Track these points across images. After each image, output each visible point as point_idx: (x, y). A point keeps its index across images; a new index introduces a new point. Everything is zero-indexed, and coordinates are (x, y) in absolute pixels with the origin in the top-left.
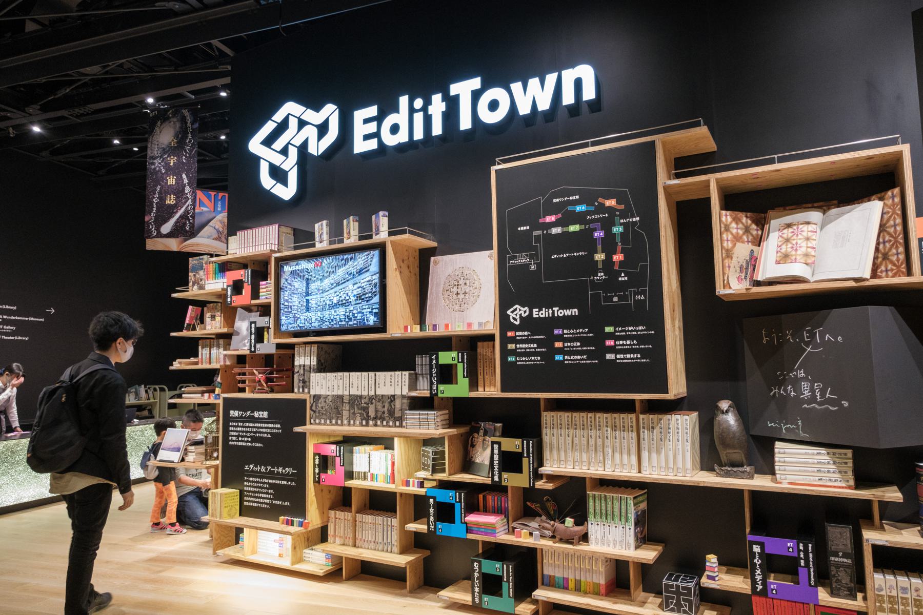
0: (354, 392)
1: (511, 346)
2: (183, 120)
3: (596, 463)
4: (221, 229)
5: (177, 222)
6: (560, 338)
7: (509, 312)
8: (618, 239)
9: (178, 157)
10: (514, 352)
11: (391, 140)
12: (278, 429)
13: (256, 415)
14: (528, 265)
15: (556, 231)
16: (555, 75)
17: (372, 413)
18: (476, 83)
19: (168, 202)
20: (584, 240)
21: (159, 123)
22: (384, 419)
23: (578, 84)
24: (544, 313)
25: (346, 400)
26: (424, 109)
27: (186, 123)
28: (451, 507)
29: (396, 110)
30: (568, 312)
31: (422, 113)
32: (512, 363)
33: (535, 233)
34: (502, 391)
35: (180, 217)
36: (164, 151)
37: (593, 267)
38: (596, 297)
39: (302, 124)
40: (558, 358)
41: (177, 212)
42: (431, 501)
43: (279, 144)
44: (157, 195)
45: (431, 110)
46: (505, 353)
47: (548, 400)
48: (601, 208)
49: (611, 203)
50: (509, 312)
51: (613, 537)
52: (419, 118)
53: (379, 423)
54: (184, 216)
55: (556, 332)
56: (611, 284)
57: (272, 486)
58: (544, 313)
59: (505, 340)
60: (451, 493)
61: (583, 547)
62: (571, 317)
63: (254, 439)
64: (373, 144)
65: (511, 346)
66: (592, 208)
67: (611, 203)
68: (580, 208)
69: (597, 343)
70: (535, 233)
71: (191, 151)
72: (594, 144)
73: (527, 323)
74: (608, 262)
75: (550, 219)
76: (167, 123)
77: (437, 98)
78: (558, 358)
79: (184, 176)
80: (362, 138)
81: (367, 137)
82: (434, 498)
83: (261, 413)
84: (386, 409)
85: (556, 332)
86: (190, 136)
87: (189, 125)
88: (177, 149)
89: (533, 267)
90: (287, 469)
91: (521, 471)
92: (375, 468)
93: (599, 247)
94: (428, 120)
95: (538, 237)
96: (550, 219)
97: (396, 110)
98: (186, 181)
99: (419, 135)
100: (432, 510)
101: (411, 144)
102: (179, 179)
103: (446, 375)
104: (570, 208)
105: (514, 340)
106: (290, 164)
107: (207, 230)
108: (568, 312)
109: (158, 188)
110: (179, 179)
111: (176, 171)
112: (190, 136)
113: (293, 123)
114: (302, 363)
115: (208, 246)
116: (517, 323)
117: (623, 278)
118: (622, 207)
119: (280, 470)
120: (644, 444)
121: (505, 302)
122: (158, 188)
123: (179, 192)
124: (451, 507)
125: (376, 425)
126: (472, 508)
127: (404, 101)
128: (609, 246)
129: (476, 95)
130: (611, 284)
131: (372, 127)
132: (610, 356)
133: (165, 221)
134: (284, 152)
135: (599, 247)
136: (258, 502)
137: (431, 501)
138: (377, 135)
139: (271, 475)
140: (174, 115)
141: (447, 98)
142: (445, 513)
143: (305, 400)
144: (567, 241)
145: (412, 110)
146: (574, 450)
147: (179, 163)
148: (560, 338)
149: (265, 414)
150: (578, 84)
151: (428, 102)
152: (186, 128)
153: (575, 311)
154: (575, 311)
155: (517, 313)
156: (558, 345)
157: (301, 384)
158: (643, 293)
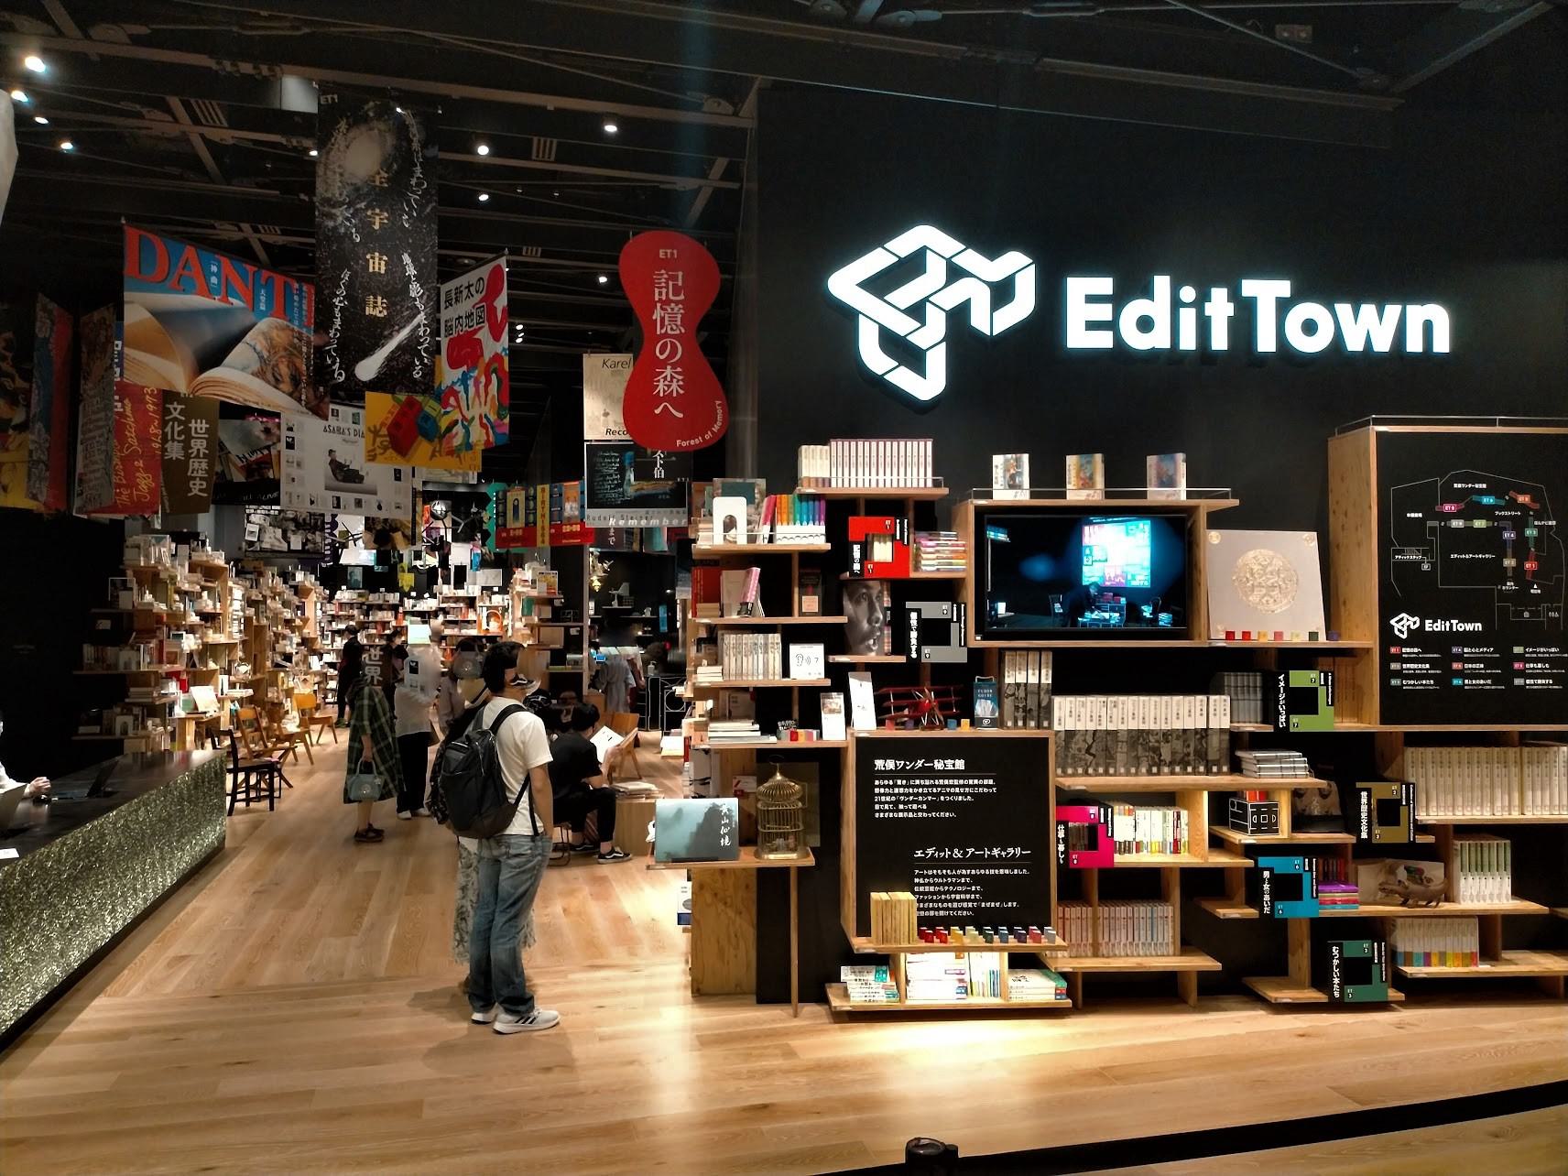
0: (1133, 726)
1: (1394, 666)
2: (401, 129)
3: (1543, 806)
4: (266, 354)
5: (390, 359)
6: (1460, 658)
7: (1393, 622)
8: (1531, 544)
9: (392, 212)
10: (1399, 674)
11: (1138, 341)
12: (988, 786)
13: (938, 765)
14: (1419, 563)
15: (1457, 524)
16: (1399, 308)
17: (1166, 755)
18: (1283, 288)
19: (369, 311)
20: (1490, 540)
21: (343, 125)
22: (1188, 764)
23: (1428, 327)
24: (1439, 626)
25: (1123, 737)
26: (1199, 304)
27: (410, 141)
28: (1297, 879)
29: (1147, 293)
30: (1469, 627)
31: (1193, 311)
32: (1396, 687)
33: (1429, 523)
34: (1383, 722)
35: (399, 347)
36: (357, 193)
37: (1502, 575)
38: (1504, 611)
39: (955, 273)
40: (1456, 682)
41: (391, 336)
42: (1266, 874)
43: (907, 294)
44: (342, 291)
45: (1209, 309)
46: (1386, 674)
47: (1407, 734)
48: (1513, 504)
49: (1523, 499)
50: (1393, 622)
51: (1487, 891)
52: (1188, 317)
53: (1177, 769)
54: (409, 347)
55: (1455, 650)
56: (1522, 597)
57: (976, 880)
58: (1439, 626)
59: (1386, 658)
60: (1298, 861)
61: (1446, 907)
62: (1474, 632)
63: (933, 806)
64: (1104, 340)
65: (1394, 666)
66: (1502, 503)
67: (1523, 499)
68: (1488, 500)
69: (1503, 666)
70: (1429, 523)
71: (422, 206)
72: (1503, 423)
73: (1417, 637)
74: (1519, 569)
75: (1448, 508)
76: (363, 128)
77: (1219, 294)
78: (1456, 682)
79: (406, 259)
80: (1083, 326)
81: (1092, 326)
82: (1271, 870)
83: (949, 762)
84: (1191, 750)
85: (1455, 650)
86: (418, 170)
87: (416, 146)
88: (391, 191)
89: (1426, 567)
90: (1011, 850)
91: (1398, 823)
92: (1146, 836)
93: (1509, 551)
94: (1204, 325)
95: (1433, 529)
96: (1448, 508)
97: (1147, 293)
98: (411, 271)
99: (1188, 342)
100: (1266, 887)
101: (1172, 356)
102: (395, 265)
103: (1304, 701)
104: (1475, 498)
105: (1399, 658)
106: (930, 335)
107: (239, 353)
108: (1469, 627)
109: (346, 275)
110: (395, 265)
111: (389, 243)
112: (418, 170)
113: (936, 269)
114: (1021, 679)
115: (242, 388)
116: (1404, 636)
117: (1535, 591)
118: (1537, 506)
119: (996, 852)
120: (1528, 782)
121: (1388, 608)
122: (346, 275)
123: (395, 290)
124: (1297, 879)
125: (1173, 773)
126: (1326, 879)
127: (1162, 283)
128: (1520, 548)
129: (1283, 306)
130: (1522, 597)
131: (1104, 312)
132: (1518, 682)
133: (367, 352)
134: (917, 311)
135: (1509, 551)
136: (947, 909)
137: (1266, 874)
138: (1112, 325)
139: (976, 862)
140: (379, 116)
141: (1235, 296)
142: (1288, 887)
143: (1046, 740)
144: (1469, 539)
145: (1176, 304)
146: (1451, 794)
147: (392, 230)
148: (1460, 658)
149: (960, 764)
150: (1428, 327)
151: (1203, 297)
152: (410, 151)
153: (1478, 627)
154: (1478, 627)
155: (1404, 624)
156: (1456, 666)
157: (1020, 714)
158: (1557, 609)
